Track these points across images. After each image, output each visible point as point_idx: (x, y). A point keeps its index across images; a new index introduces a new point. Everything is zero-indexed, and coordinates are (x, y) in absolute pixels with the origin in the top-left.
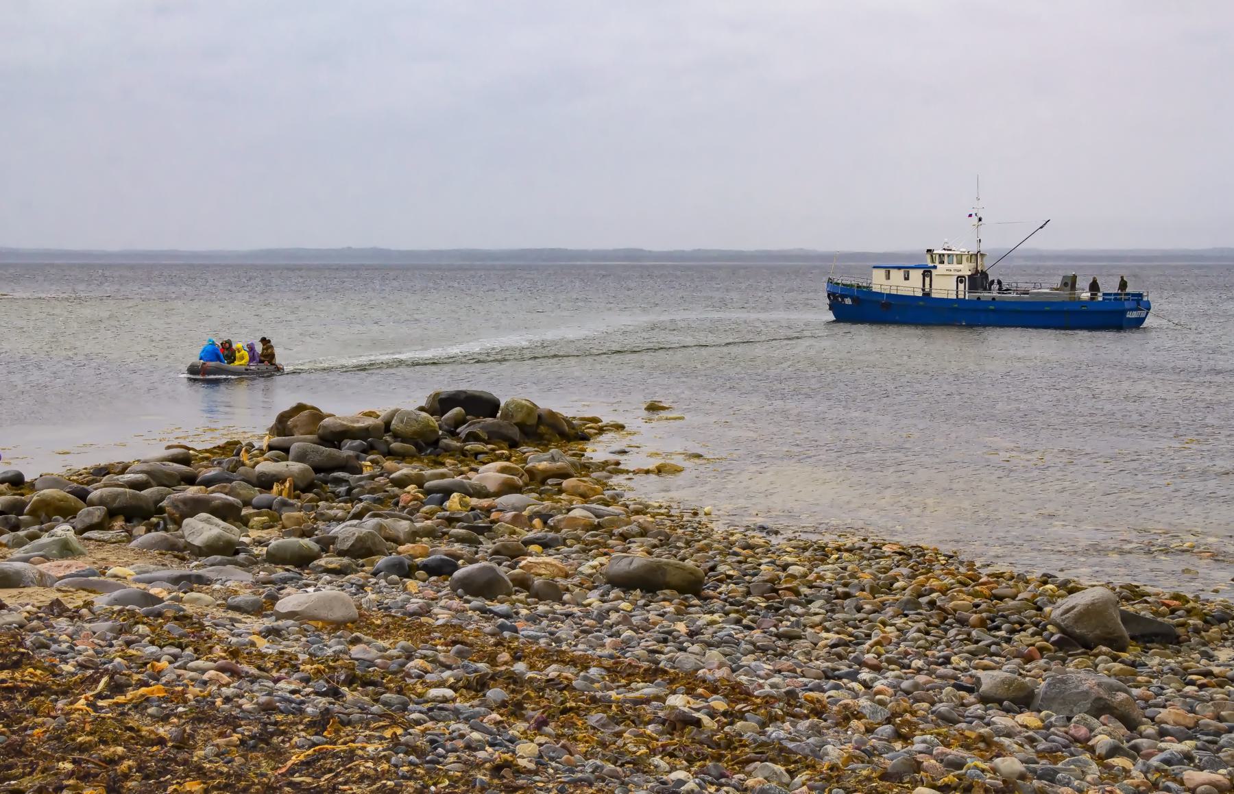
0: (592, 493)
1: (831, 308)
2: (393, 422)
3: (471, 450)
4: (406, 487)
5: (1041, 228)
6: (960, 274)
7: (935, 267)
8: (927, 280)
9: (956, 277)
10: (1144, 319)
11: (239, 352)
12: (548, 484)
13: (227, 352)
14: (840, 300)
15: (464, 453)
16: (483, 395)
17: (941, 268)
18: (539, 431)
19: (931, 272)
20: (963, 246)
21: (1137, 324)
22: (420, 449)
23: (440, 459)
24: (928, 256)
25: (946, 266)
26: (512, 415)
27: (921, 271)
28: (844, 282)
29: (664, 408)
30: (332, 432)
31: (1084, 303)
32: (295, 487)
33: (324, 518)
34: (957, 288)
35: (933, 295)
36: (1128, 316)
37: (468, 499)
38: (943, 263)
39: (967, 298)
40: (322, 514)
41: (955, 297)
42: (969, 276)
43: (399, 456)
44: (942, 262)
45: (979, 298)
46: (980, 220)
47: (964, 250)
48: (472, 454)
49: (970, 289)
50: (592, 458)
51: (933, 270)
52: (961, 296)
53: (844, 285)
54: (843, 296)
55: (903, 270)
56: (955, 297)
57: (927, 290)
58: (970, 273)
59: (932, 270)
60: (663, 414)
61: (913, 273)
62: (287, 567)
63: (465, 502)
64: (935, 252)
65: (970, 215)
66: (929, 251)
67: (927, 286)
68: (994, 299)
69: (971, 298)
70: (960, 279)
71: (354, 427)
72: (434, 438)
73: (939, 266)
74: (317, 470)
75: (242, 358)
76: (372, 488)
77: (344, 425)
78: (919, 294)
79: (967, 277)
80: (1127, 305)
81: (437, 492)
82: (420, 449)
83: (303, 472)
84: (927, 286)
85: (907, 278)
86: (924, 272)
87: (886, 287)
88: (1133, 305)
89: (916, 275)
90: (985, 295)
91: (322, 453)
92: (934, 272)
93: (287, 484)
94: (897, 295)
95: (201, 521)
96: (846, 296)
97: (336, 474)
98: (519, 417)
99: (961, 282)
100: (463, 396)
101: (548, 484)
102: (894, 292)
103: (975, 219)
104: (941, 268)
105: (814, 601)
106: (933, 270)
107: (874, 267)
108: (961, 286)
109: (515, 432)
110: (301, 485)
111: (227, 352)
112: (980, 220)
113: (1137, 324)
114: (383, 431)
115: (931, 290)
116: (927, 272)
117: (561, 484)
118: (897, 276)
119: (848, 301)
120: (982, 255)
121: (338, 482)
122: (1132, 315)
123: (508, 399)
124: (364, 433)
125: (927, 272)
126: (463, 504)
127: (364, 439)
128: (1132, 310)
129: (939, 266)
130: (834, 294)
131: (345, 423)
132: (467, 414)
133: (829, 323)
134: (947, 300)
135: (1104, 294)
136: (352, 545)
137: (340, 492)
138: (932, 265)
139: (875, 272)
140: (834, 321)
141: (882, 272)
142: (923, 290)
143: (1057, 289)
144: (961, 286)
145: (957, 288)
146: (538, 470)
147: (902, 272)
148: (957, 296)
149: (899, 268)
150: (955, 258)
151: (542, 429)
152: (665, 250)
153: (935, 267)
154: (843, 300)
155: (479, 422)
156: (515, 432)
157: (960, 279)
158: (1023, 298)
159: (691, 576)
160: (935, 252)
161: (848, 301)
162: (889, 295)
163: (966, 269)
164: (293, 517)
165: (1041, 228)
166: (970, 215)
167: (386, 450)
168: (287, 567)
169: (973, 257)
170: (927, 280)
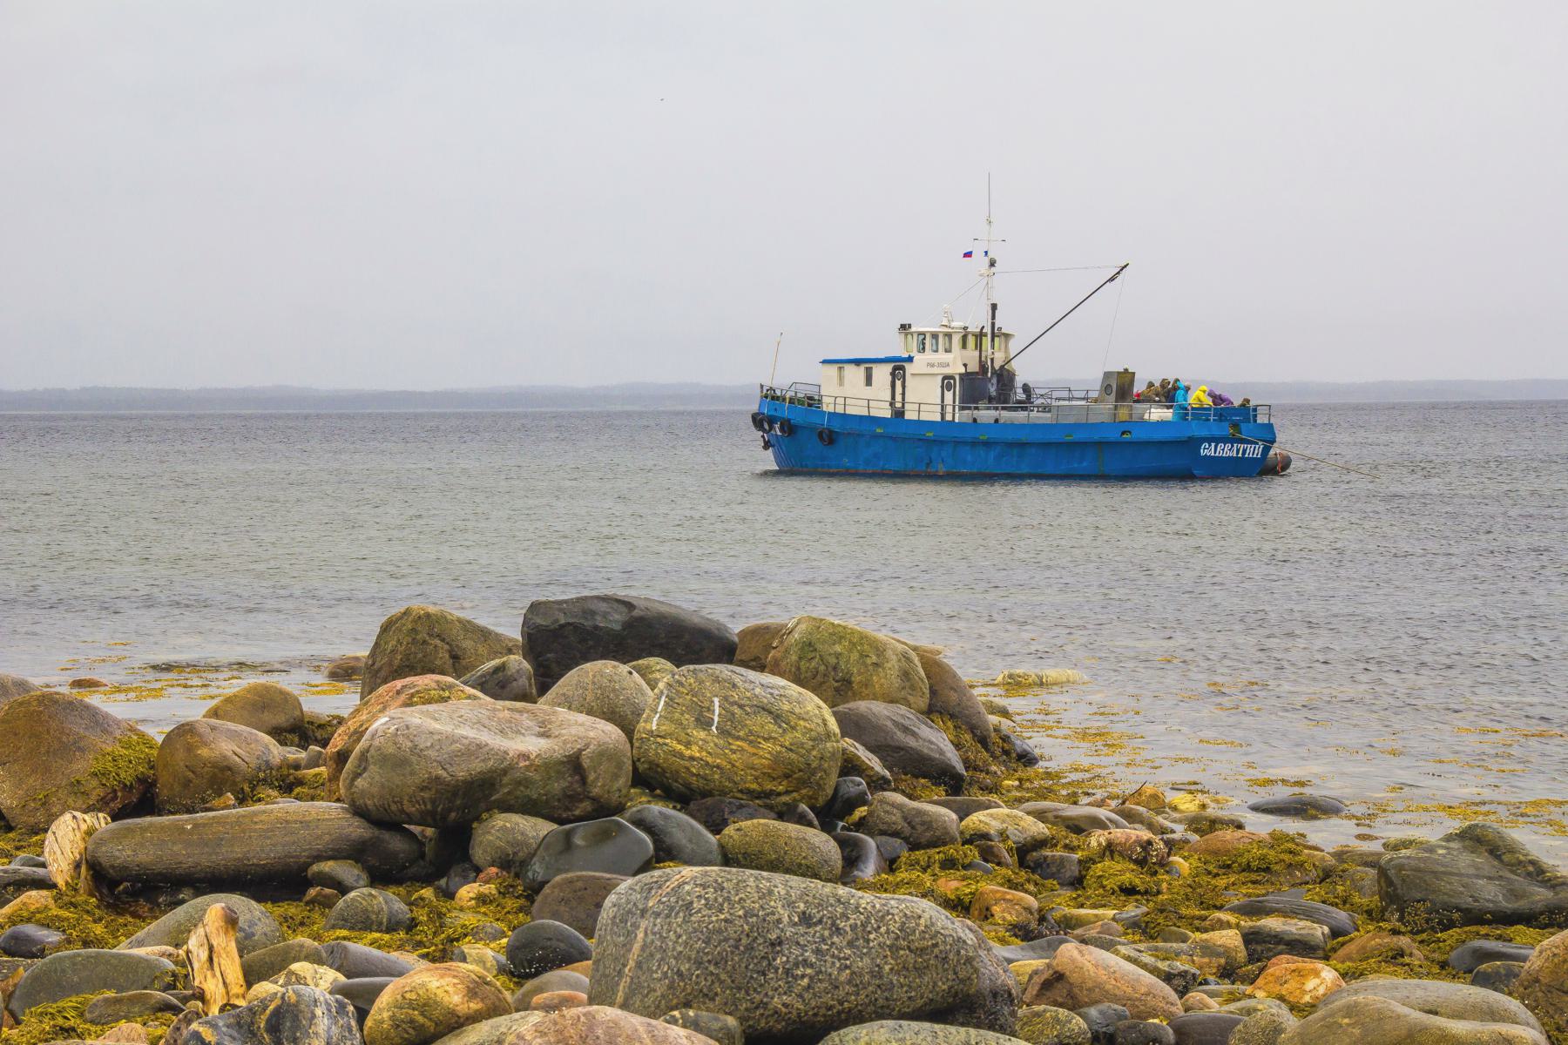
5: (1112, 279)
7: (910, 359)
9: (940, 378)
19: (903, 368)
25: (929, 356)
27: (889, 368)
30: (1033, 837)
39: (957, 421)
41: (938, 418)
46: (992, 264)
49: (962, 400)
51: (907, 366)
52: (949, 417)
55: (862, 368)
57: (898, 405)
65: (968, 255)
66: (904, 327)
67: (898, 398)
78: (887, 413)
85: (869, 381)
86: (895, 369)
89: (882, 374)
91: (862, 931)
92: (909, 368)
94: (844, 415)
95: (1029, 813)
102: (840, 410)
103: (980, 262)
105: (1013, 1034)
106: (907, 366)
108: (949, 395)
112: (992, 264)
115: (903, 404)
118: (855, 374)
125: (899, 367)
129: (918, 357)
133: (766, 474)
142: (892, 404)
144: (949, 395)
148: (943, 415)
149: (857, 362)
150: (915, 336)
153: (910, 359)
159: (1466, 861)
160: (913, 329)
163: (957, 361)
165: (1112, 279)
166: (968, 255)
170: (898, 383)
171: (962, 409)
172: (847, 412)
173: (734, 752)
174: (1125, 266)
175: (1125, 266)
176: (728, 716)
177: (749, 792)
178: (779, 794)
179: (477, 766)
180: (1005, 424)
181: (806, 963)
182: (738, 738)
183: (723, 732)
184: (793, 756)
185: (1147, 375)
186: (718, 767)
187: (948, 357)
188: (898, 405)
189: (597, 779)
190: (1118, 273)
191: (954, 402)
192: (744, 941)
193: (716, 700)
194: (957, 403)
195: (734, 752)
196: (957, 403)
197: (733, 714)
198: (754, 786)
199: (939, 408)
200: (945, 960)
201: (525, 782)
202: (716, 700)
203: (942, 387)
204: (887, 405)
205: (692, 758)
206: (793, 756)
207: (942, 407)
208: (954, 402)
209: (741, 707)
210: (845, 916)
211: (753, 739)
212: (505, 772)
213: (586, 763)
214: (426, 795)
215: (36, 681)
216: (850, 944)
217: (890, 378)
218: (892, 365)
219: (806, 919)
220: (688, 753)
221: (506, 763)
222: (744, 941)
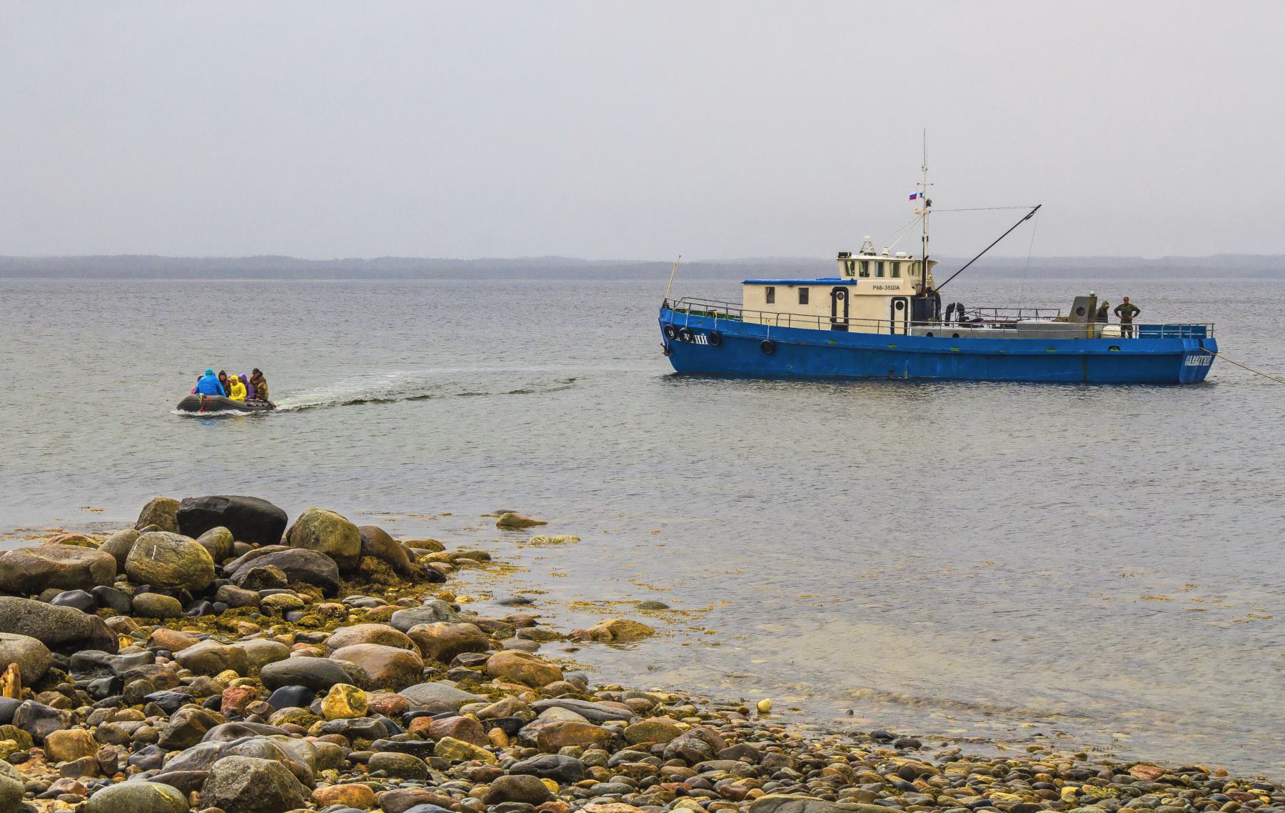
0: (543, 677)
1: (669, 351)
2: (131, 555)
3: (276, 603)
4: (217, 673)
5: (1028, 217)
6: (897, 293)
7: (853, 283)
8: (840, 304)
10: (1206, 369)
11: (235, 384)
12: (460, 663)
13: (224, 383)
14: (687, 337)
15: (264, 610)
16: (245, 502)
17: (864, 285)
18: (364, 566)
19: (846, 291)
20: (904, 249)
21: (1197, 379)
22: (187, 604)
23: (223, 620)
24: (841, 265)
25: (873, 280)
26: (317, 540)
27: (830, 289)
28: (694, 308)
29: (532, 524)
30: (23, 575)
31: (1113, 343)
32: (22, 680)
33: (112, 738)
34: (893, 317)
35: (851, 330)
36: (1188, 363)
37: (361, 694)
38: (867, 275)
39: (909, 334)
40: (108, 732)
42: (912, 297)
43: (152, 617)
44: (865, 274)
45: (930, 334)
46: (928, 203)
47: (903, 254)
48: (277, 611)
49: (913, 318)
50: (476, 614)
52: (899, 331)
53: (692, 312)
54: (692, 332)
56: (887, 332)
57: (840, 320)
58: (914, 292)
59: (848, 287)
60: (536, 533)
61: (813, 292)
62: (927, 767)
63: (356, 700)
64: (853, 257)
65: (913, 197)
66: (843, 255)
67: (840, 313)
68: (956, 335)
69: (917, 334)
70: (898, 302)
71: (62, 566)
72: (206, 581)
73: (861, 281)
74: (53, 644)
75: (239, 391)
76: (159, 678)
77: (47, 563)
79: (909, 299)
80: (1187, 345)
81: (292, 682)
82: (187, 604)
83: (31, 654)
84: (840, 313)
86: (835, 290)
87: (770, 316)
88: (1194, 345)
89: (821, 296)
90: (941, 329)
91: (46, 616)
92: (852, 291)
93: (10, 677)
94: (789, 329)
96: (699, 331)
97: (82, 654)
98: (332, 541)
99: (900, 306)
100: (222, 507)
101: (460, 663)
103: (920, 202)
104: (864, 285)
107: (746, 283)
108: (900, 314)
109: (327, 568)
110: (33, 678)
111: (224, 383)
112: (928, 203)
113: (1197, 379)
114: (114, 571)
115: (846, 321)
116: (840, 291)
117: (483, 662)
118: (789, 298)
119: (702, 340)
120: (931, 263)
121: (89, 667)
122: (1192, 362)
123: (306, 510)
124: (82, 577)
125: (840, 291)
126: (357, 705)
127: (86, 585)
128: (1193, 353)
130: (676, 329)
131: (44, 558)
132: (235, 540)
134: (878, 336)
135: (1142, 327)
136: (246, 791)
137: (97, 687)
138: (849, 278)
139: (747, 289)
140: (674, 375)
141: (761, 291)
142: (833, 320)
143: (1066, 320)
144: (900, 314)
145: (893, 317)
146: (432, 637)
147: (795, 291)
148: (906, 331)
149: (791, 284)
151: (370, 563)
152: (172, 255)
153: (853, 283)
154: (692, 338)
155: (266, 553)
156: (327, 568)
157: (898, 302)
158: (1008, 334)
161: (702, 340)
162: (775, 329)
163: (906, 285)
164: (70, 739)
165: (1028, 217)
166: (913, 197)
167: (127, 607)
168: (927, 767)
169: (917, 264)
170: (840, 304)
171: (913, 324)
172: (779, 325)
173: (159, 567)
174: (1039, 207)
175: (1039, 207)
176: (159, 553)
177: (165, 583)
178: (176, 585)
179: (41, 570)
180: (964, 339)
181: (27, 625)
182: (161, 562)
183: (155, 559)
184: (181, 569)
185: (1111, 298)
186: (152, 573)
187: (896, 281)
188: (840, 320)
189: (97, 577)
190: (1033, 212)
191: (906, 318)
192: (9, 618)
193: (155, 546)
194: (909, 320)
195: (159, 567)
196: (909, 320)
197: (161, 552)
198: (166, 581)
199: (889, 324)
200: (74, 626)
201: (63, 577)
202: (155, 546)
203: (892, 307)
204: (828, 320)
205: (143, 569)
206: (181, 569)
207: (893, 324)
208: (906, 318)
209: (164, 549)
210: (42, 611)
211: (166, 562)
212: (54, 573)
213: (91, 570)
214: (19, 580)
215: (359, 523)
216: (42, 620)
217: (831, 298)
218: (833, 287)
219: (29, 612)
220: (141, 567)
221: (54, 569)
222: (9, 618)
